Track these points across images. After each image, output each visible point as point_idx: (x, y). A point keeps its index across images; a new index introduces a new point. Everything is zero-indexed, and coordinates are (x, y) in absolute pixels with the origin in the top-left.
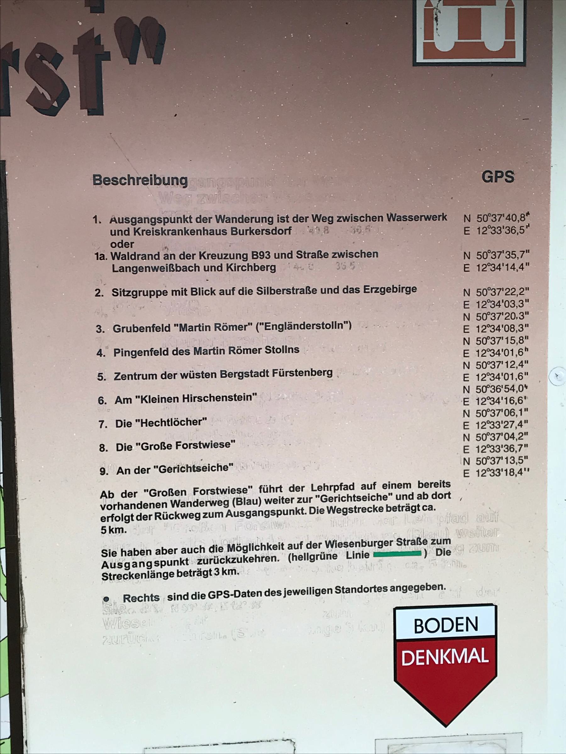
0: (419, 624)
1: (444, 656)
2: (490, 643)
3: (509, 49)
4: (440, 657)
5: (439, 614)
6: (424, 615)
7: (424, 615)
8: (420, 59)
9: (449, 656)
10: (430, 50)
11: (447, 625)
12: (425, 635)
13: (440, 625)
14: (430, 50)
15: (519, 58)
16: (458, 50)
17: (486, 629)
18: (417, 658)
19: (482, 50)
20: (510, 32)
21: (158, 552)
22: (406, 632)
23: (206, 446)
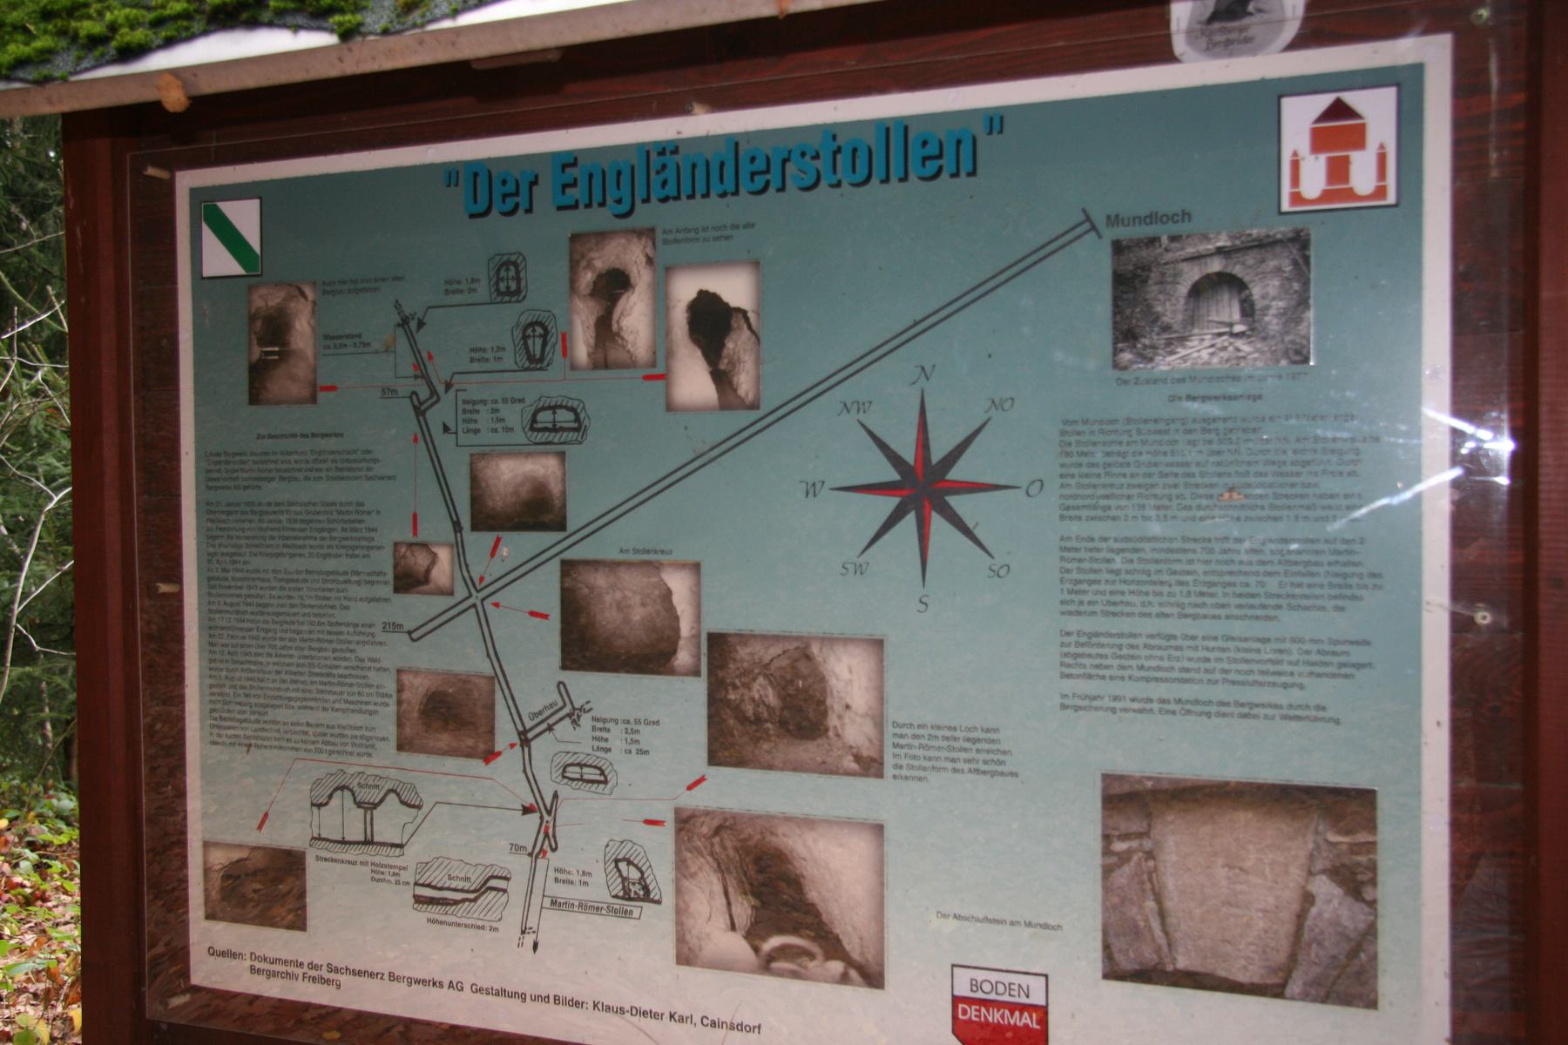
0: (975, 985)
1: (997, 1016)
2: (1042, 1012)
3: (1380, 192)
4: (994, 1016)
5: (994, 977)
6: (980, 976)
7: (980, 976)
8: (1286, 207)
9: (1003, 1017)
10: (1297, 198)
11: (1001, 988)
12: (980, 995)
13: (994, 986)
14: (1297, 198)
15: (1391, 198)
16: (1326, 196)
17: (1037, 999)
18: (972, 1013)
19: (1350, 194)
20: (1382, 173)
21: (1204, 638)
22: (963, 990)
23: (644, 1013)
